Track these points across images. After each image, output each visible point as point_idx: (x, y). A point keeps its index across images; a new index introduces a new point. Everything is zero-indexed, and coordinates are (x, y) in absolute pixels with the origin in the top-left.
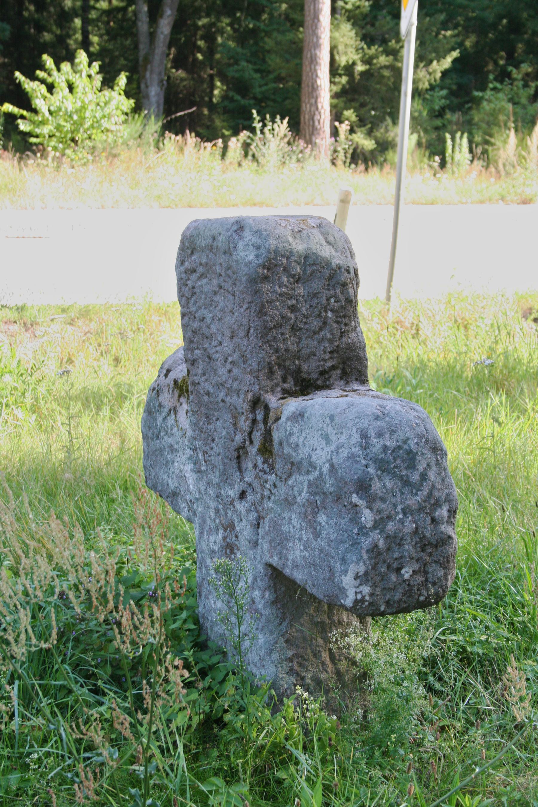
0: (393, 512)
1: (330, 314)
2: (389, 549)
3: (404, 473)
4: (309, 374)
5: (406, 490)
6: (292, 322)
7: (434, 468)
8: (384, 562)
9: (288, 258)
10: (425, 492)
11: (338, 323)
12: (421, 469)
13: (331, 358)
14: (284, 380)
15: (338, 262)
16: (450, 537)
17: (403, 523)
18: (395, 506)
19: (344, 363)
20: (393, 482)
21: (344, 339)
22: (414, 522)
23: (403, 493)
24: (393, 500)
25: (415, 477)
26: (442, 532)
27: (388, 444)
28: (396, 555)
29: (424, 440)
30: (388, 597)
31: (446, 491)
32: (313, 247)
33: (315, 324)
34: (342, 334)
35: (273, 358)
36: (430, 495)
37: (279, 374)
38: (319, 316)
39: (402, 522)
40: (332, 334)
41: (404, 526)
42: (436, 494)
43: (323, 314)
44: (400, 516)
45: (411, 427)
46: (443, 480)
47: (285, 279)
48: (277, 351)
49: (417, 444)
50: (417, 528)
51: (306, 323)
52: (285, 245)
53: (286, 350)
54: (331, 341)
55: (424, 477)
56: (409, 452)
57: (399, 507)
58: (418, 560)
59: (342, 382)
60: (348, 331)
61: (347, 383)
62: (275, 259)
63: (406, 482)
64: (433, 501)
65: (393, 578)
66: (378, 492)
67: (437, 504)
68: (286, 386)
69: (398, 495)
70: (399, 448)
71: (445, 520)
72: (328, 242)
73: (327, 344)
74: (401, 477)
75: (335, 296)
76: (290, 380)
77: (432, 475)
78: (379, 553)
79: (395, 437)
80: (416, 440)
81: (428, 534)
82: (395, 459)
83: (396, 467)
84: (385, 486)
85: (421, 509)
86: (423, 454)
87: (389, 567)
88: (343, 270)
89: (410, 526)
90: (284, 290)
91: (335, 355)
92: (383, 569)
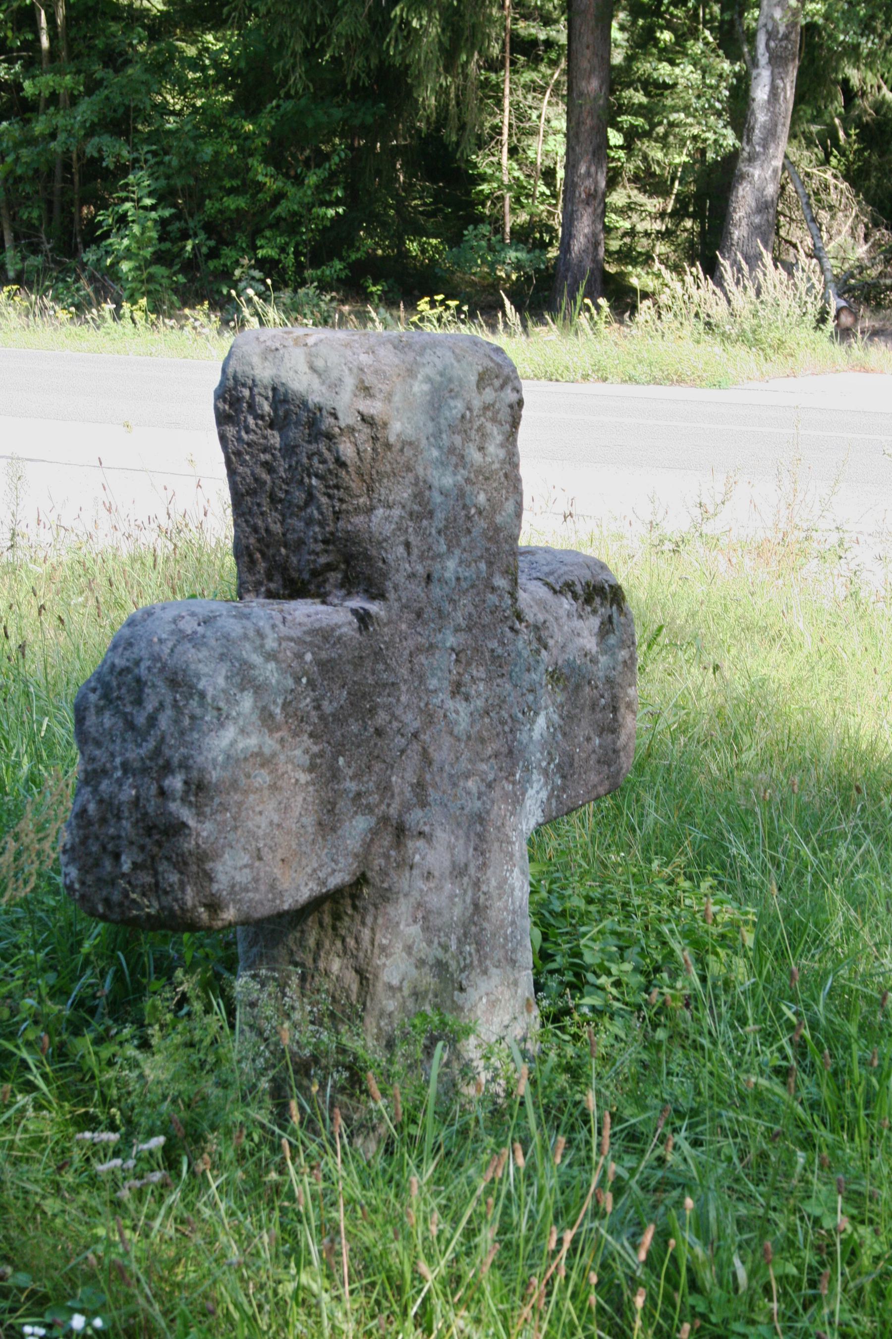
0: (108, 765)
1: (314, 481)
2: (103, 821)
3: (128, 709)
4: (300, 572)
5: (129, 735)
6: (268, 487)
7: (169, 712)
8: (97, 838)
9: (251, 389)
10: (151, 744)
11: (330, 497)
12: (150, 707)
13: (326, 551)
14: (270, 578)
15: (317, 400)
16: (184, 825)
17: (121, 785)
18: (113, 755)
19: (347, 562)
20: (114, 720)
21: (341, 524)
22: (135, 787)
23: (124, 740)
24: (111, 748)
25: (141, 720)
26: (170, 813)
27: (117, 661)
28: (112, 831)
29: (159, 665)
30: (104, 893)
31: (182, 750)
32: (283, 374)
33: (299, 496)
34: (337, 515)
35: (252, 540)
36: (157, 752)
37: (262, 566)
38: (301, 482)
39: (120, 783)
40: (321, 513)
41: (120, 790)
42: (167, 752)
43: (306, 480)
44: (119, 774)
45: (150, 643)
46: (182, 733)
47: (251, 421)
48: (255, 530)
49: (149, 669)
50: (137, 798)
51: (287, 492)
52: (246, 368)
53: (267, 530)
54: (322, 524)
55: (152, 720)
56: (138, 680)
57: (118, 760)
58: (142, 848)
59: (343, 592)
60: (348, 512)
61: (349, 594)
62: (235, 389)
63: (130, 725)
64: (161, 762)
65: (108, 864)
66: (92, 730)
67: (167, 769)
68: (272, 586)
69: (118, 741)
70: (127, 670)
71: (179, 795)
72: (313, 368)
73: (317, 529)
74: (125, 715)
75: (319, 453)
76: (277, 577)
77: (164, 721)
78: (90, 823)
79: (127, 654)
80: (148, 663)
81: (151, 810)
82: (119, 687)
83: (119, 698)
84: (102, 724)
85: (145, 770)
86: (154, 686)
87: (104, 848)
88: (324, 413)
89: (128, 793)
90: (252, 437)
91: (331, 547)
92: (95, 848)
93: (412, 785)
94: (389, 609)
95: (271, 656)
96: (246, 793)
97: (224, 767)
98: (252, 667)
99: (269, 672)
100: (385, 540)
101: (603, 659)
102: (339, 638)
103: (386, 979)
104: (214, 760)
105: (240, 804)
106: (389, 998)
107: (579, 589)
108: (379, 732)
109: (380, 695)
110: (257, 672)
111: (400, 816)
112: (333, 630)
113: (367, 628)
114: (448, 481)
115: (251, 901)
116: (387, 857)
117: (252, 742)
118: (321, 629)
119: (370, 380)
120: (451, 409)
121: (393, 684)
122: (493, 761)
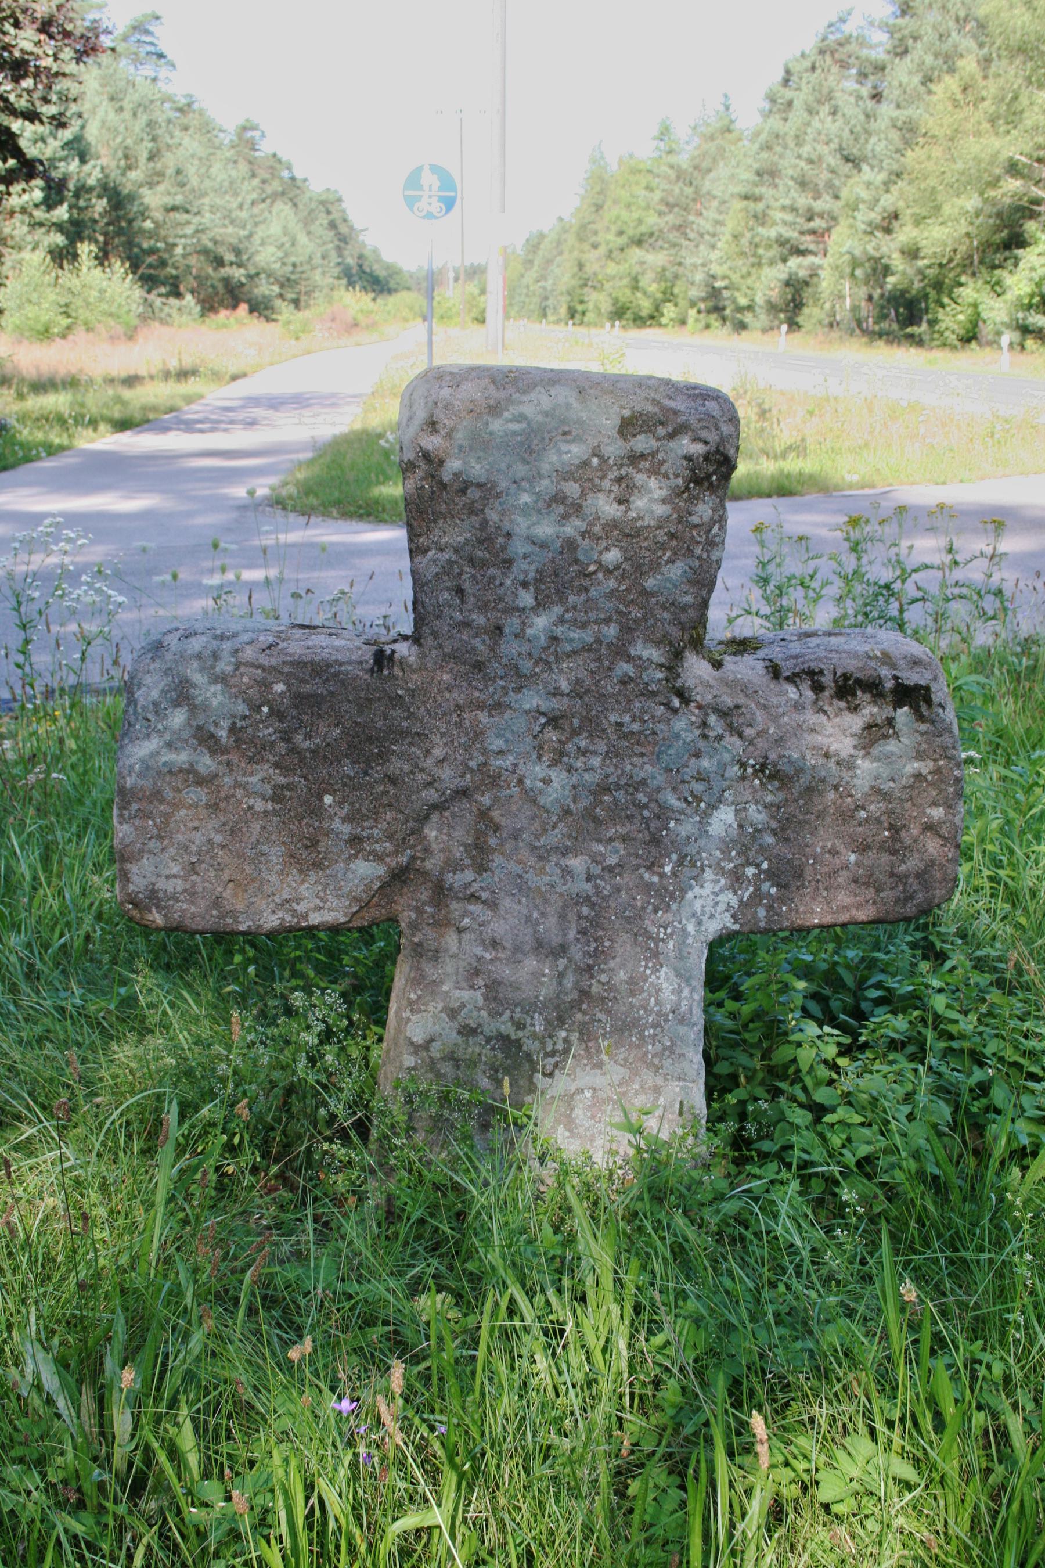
93: (466, 846)
94: (422, 656)
95: (222, 679)
96: (176, 806)
97: (140, 775)
98: (194, 686)
99: (214, 696)
100: (427, 584)
101: (865, 765)
102: (336, 675)
103: (408, 1034)
104: (131, 767)
105: (167, 817)
106: (411, 1054)
107: (827, 680)
108: (393, 780)
109: (395, 742)
110: (197, 692)
111: (442, 873)
112: (329, 665)
113: (381, 670)
114: (545, 529)
115: (183, 911)
116: (419, 911)
117: (181, 758)
118: (312, 663)
119: (440, 414)
120: (560, 453)
121: (418, 734)
122: (617, 844)
